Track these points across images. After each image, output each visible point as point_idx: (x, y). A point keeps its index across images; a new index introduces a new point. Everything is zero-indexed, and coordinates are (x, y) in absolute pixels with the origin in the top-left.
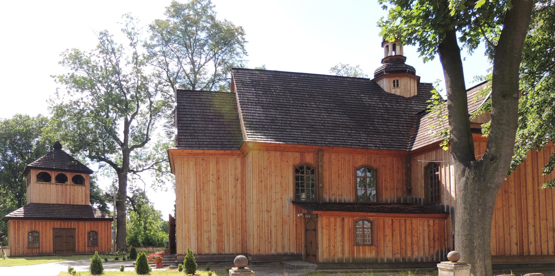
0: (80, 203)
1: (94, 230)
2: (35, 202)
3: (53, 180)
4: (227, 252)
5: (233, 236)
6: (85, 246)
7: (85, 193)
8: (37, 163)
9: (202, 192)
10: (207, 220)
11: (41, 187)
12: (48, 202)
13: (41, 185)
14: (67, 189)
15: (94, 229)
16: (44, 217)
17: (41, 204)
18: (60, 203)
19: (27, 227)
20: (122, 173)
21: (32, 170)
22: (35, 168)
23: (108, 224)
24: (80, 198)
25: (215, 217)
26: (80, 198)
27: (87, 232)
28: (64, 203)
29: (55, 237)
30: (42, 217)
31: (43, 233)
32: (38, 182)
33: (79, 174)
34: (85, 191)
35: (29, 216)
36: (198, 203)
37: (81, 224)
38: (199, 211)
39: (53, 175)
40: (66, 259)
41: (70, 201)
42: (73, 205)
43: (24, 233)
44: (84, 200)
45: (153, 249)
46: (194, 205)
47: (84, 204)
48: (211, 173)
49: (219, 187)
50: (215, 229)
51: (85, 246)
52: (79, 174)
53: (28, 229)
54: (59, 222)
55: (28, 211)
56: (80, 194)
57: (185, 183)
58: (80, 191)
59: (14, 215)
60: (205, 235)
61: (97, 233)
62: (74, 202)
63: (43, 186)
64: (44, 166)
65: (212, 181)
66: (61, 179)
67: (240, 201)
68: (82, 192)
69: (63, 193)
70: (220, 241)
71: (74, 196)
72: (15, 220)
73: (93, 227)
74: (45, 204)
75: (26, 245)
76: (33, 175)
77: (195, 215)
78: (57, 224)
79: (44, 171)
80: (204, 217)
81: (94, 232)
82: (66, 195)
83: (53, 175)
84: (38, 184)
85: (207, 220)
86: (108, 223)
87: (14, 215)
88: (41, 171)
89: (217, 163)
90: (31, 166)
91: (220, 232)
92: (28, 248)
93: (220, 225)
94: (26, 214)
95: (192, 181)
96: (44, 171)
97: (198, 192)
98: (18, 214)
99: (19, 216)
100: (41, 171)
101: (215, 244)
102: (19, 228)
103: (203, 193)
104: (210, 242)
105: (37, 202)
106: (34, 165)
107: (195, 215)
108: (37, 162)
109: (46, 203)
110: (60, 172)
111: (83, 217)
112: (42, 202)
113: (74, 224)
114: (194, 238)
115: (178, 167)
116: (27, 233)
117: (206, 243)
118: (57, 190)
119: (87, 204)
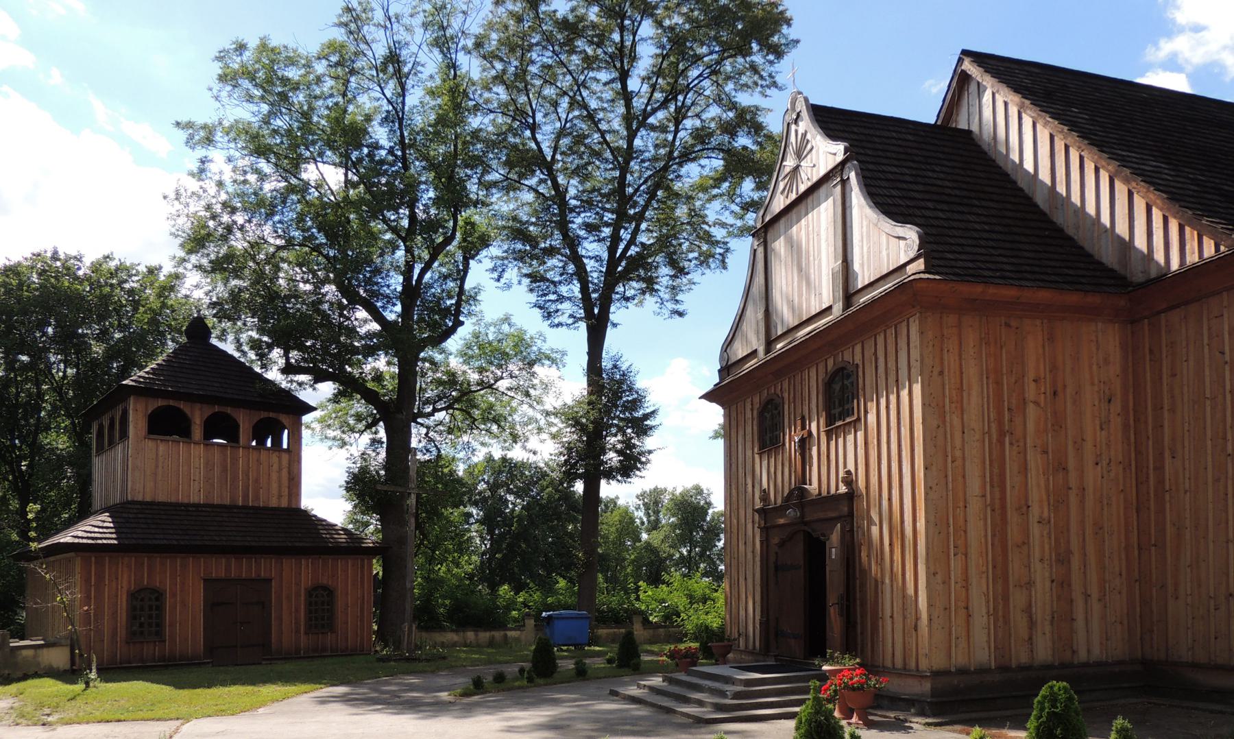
0: (274, 503)
1: (325, 582)
2: (140, 499)
3: (197, 432)
4: (1082, 656)
5: (1099, 600)
6: (298, 631)
7: (289, 473)
8: (149, 378)
9: (1007, 439)
10: (1024, 543)
11: (160, 453)
12: (181, 498)
13: (162, 448)
14: (237, 460)
15: (324, 581)
16: (182, 543)
17: (159, 504)
18: (216, 501)
19: (125, 576)
20: (400, 416)
21: (132, 398)
22: (140, 391)
23: (363, 567)
24: (275, 486)
25: (1045, 533)
26: (275, 486)
27: (305, 589)
28: (227, 502)
29: (212, 606)
30: (175, 543)
31: (174, 595)
32: (152, 436)
33: (271, 415)
34: (289, 468)
35: (134, 542)
36: (998, 481)
37: (288, 564)
38: (998, 511)
39: (198, 417)
40: (550, 708)
41: (246, 496)
42: (253, 508)
43: (117, 596)
44: (285, 492)
45: (477, 635)
46: (984, 487)
47: (284, 504)
48: (1031, 375)
49: (1057, 423)
50: (1047, 574)
51: (298, 631)
52: (271, 415)
53: (129, 582)
54: (224, 560)
55: (127, 525)
56: (274, 476)
57: (953, 405)
58: (276, 467)
59: (88, 538)
60: (1018, 599)
61: (332, 592)
62: (257, 497)
63: (164, 450)
64: (172, 387)
65: (1036, 403)
66: (220, 426)
67: (1121, 477)
68: (280, 470)
69: (224, 470)
70: (1063, 618)
71: (257, 481)
72: (87, 554)
73: (322, 575)
74: (170, 504)
75: (122, 633)
76: (137, 416)
77: (986, 524)
78: (219, 567)
79: (172, 403)
80: (1013, 533)
81: (325, 588)
82: (235, 479)
83: (198, 417)
84: (150, 444)
85: (1024, 543)
86: (363, 560)
87: (88, 538)
88: (160, 403)
89: (1051, 338)
90: (133, 384)
91: (1062, 584)
92: (127, 643)
93: (1062, 558)
94: (123, 535)
95: (974, 401)
96: (172, 403)
97: (994, 441)
98: (99, 535)
99: (105, 542)
100: (160, 403)
101: (1048, 628)
102: (100, 578)
103: (1011, 444)
104: (1032, 624)
105: (148, 499)
106: (140, 382)
107: (986, 524)
108: (146, 373)
109: (173, 500)
110: (217, 409)
111: (297, 544)
112: (161, 498)
113: (264, 567)
114: (984, 611)
115: (930, 348)
116: (125, 597)
117: (1019, 621)
118: (207, 464)
119: (294, 506)
